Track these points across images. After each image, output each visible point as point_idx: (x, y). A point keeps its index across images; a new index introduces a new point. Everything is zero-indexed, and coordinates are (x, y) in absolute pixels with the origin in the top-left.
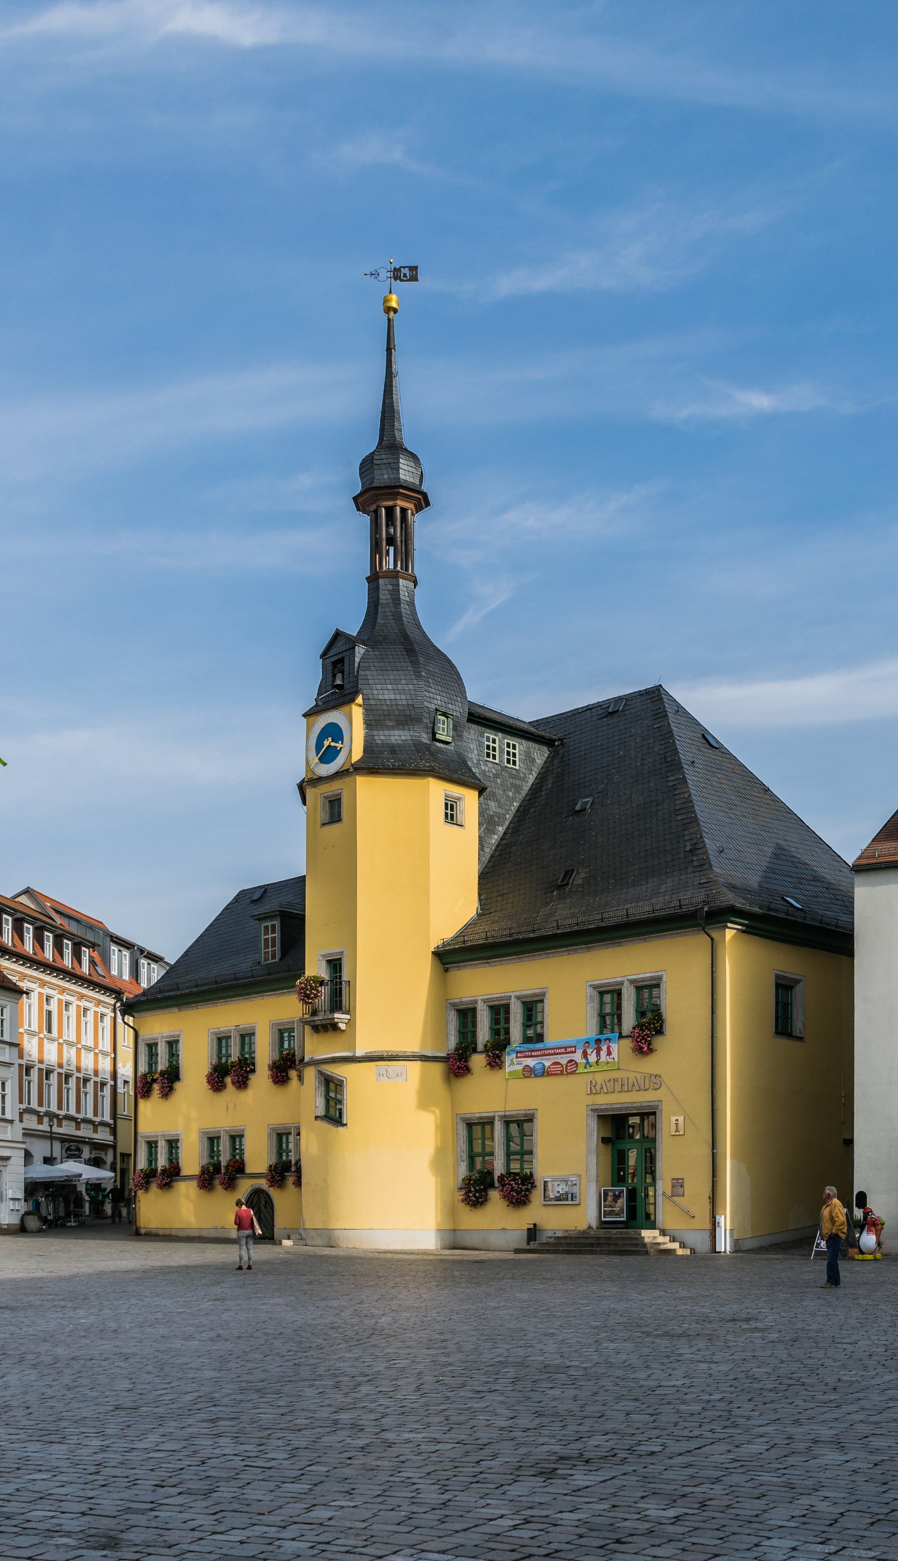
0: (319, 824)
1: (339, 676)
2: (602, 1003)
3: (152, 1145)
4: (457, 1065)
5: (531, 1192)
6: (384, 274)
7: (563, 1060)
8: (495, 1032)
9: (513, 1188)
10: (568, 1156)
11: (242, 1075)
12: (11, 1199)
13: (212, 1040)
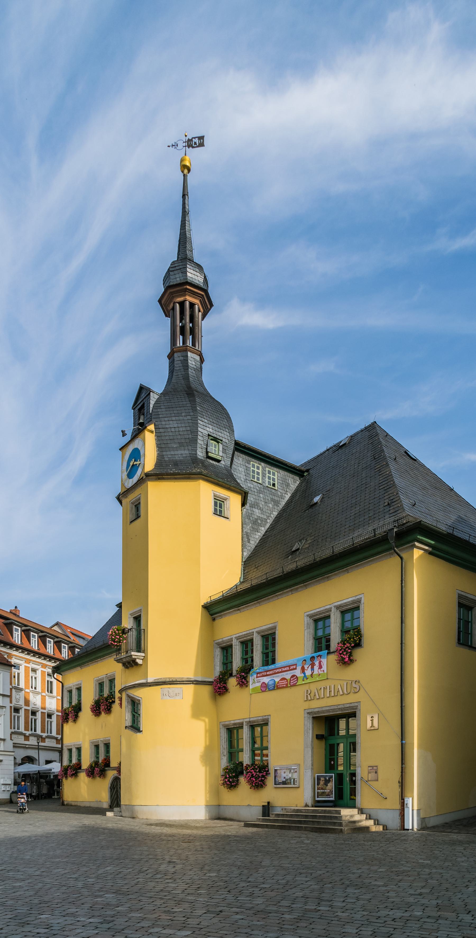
0: (129, 523)
1: (142, 417)
2: (316, 629)
3: (70, 750)
4: (219, 687)
5: (265, 778)
6: (181, 145)
7: (288, 675)
8: (245, 660)
9: (252, 775)
10: (292, 750)
11: (107, 705)
12: (3, 784)
13: (96, 685)
